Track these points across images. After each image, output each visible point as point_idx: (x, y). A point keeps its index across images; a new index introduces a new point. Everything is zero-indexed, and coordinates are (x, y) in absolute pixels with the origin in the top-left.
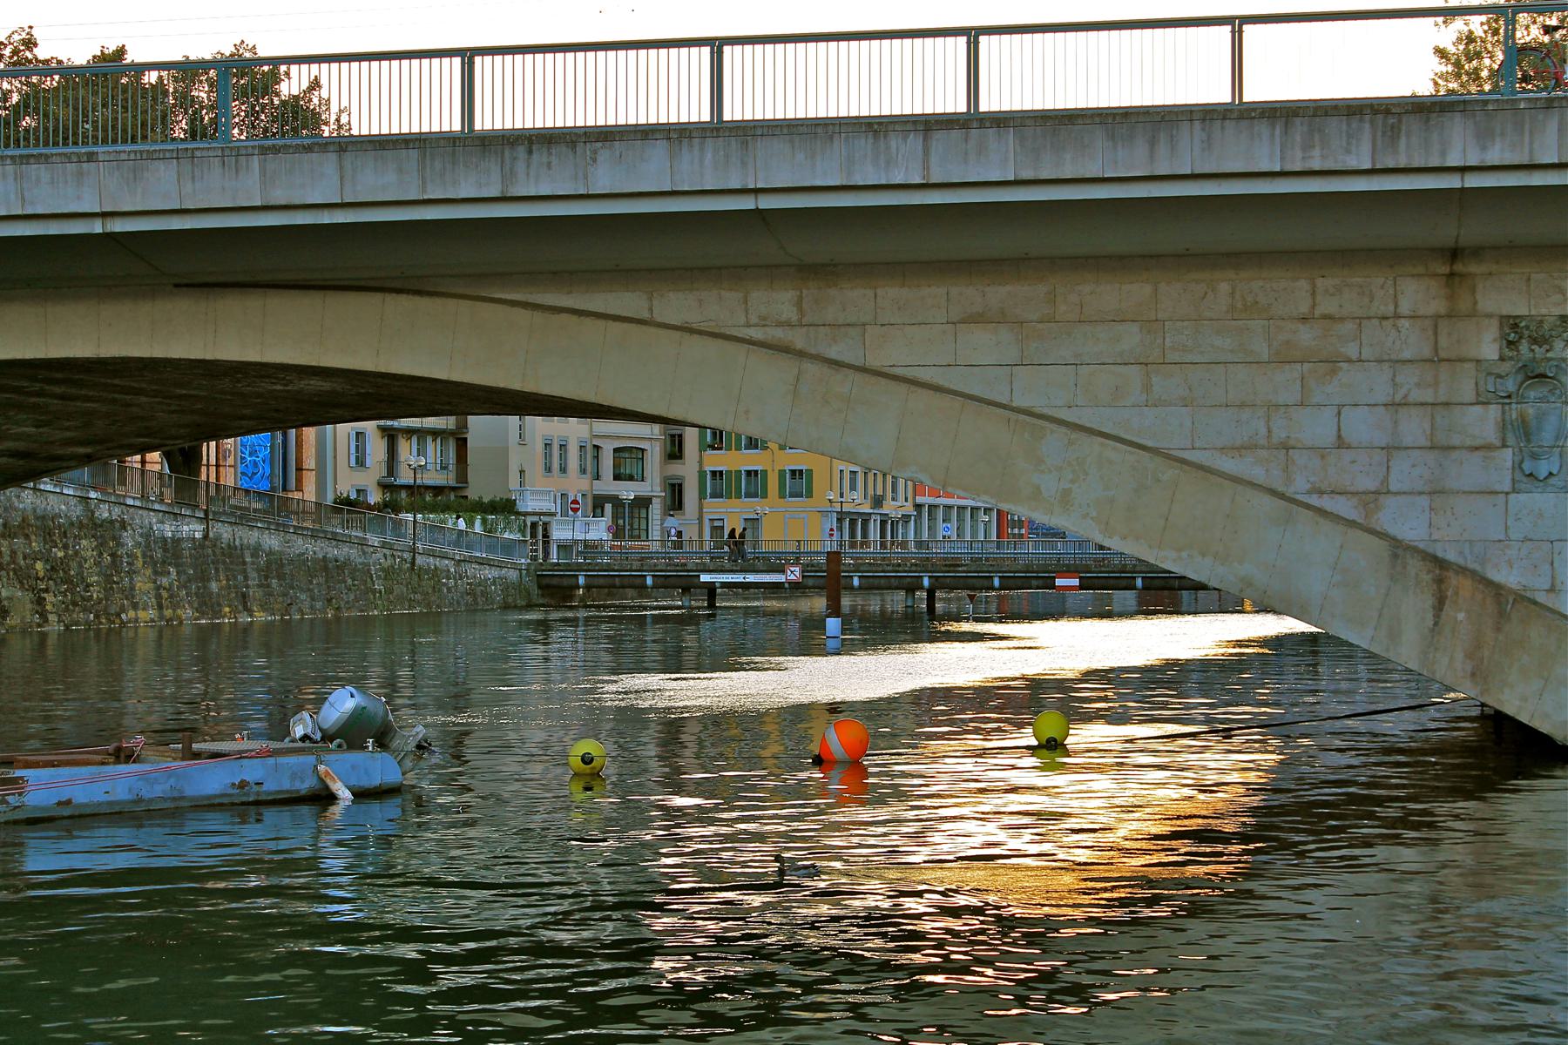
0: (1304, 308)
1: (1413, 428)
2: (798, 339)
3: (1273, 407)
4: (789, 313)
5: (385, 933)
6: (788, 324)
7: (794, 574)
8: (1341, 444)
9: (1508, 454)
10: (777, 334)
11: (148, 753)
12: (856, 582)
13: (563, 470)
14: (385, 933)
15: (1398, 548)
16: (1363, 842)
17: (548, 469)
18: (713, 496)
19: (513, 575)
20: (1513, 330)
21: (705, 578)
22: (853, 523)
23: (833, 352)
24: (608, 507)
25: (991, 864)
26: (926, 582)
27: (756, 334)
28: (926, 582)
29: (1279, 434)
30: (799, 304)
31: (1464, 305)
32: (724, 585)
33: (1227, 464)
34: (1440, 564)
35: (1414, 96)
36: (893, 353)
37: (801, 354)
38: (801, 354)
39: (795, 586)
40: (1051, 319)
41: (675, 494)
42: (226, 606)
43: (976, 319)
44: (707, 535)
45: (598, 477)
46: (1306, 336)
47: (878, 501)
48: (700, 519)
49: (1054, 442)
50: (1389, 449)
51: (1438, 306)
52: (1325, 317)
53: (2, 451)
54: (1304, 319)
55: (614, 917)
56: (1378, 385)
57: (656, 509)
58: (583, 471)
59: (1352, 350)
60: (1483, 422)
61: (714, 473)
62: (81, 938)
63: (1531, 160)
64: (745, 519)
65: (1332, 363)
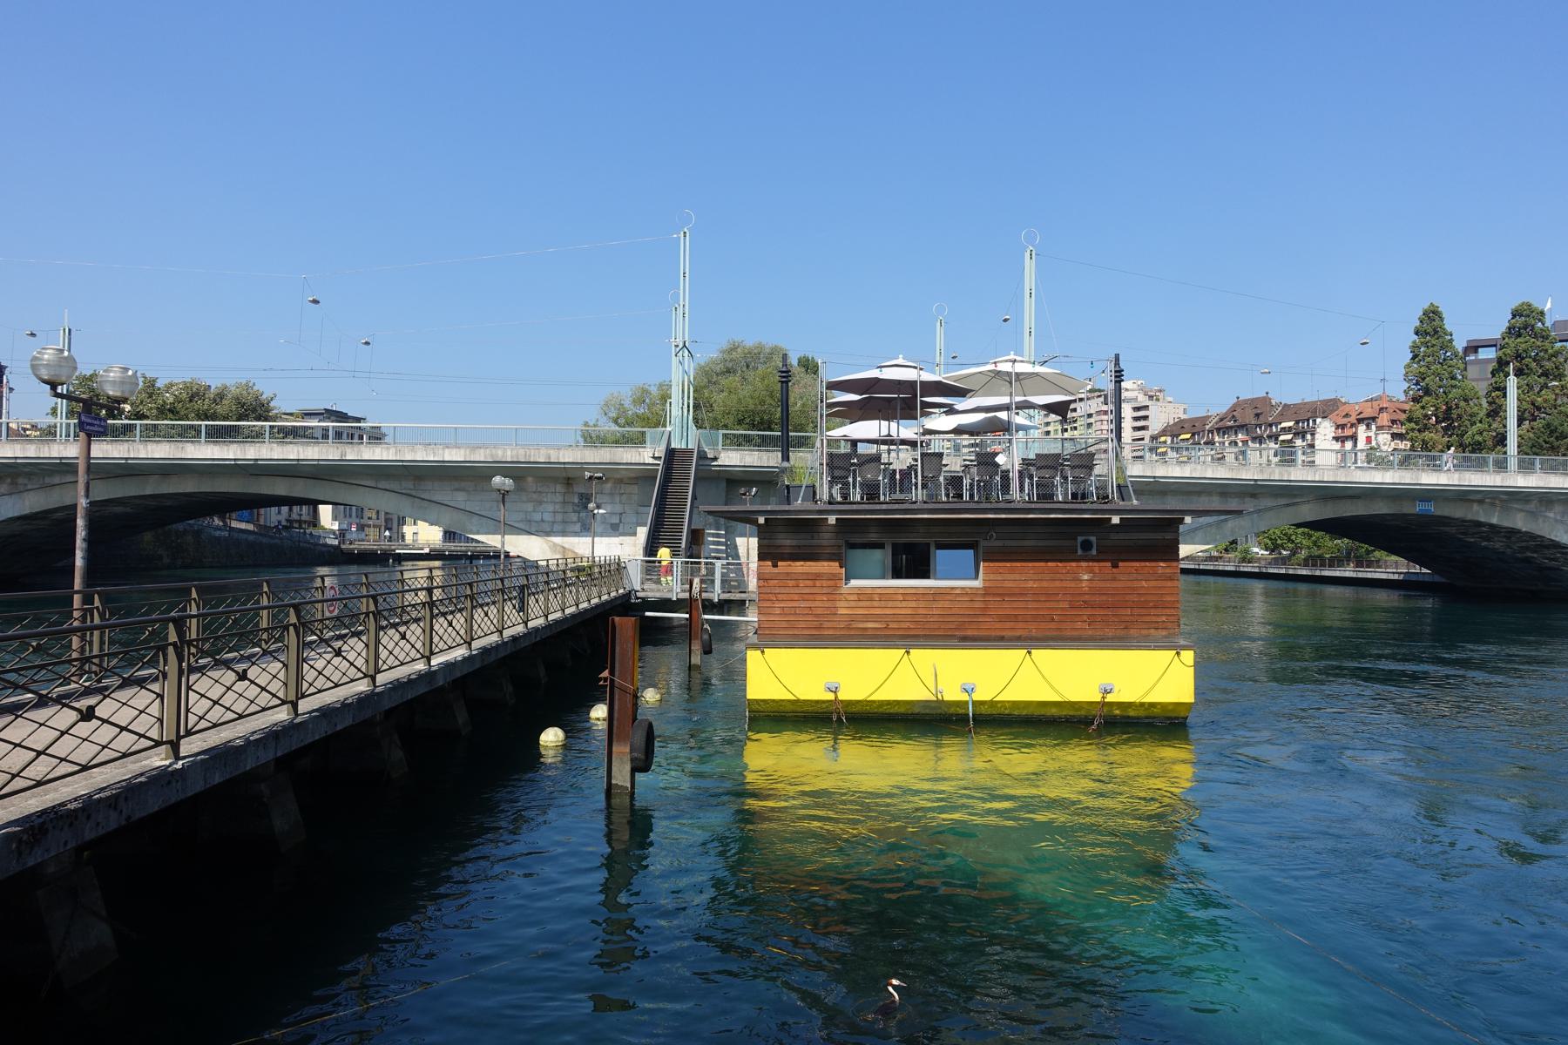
0: (534, 490)
1: (559, 517)
2: (414, 493)
3: (526, 512)
4: (412, 487)
5: (971, 720)
6: (411, 489)
8: (542, 521)
10: (408, 492)
13: (350, 516)
14: (971, 720)
16: (1295, 496)
17: (345, 516)
23: (422, 496)
27: (404, 491)
29: (528, 517)
30: (414, 484)
31: (571, 490)
33: (517, 525)
36: (437, 498)
37: (415, 497)
38: (415, 497)
40: (476, 490)
42: (1271, 430)
43: (457, 490)
45: (362, 518)
46: (535, 496)
49: (475, 519)
50: (554, 522)
51: (563, 491)
52: (540, 492)
54: (535, 492)
55: (868, 882)
56: (550, 508)
58: (357, 517)
59: (545, 500)
62: (565, 850)
63: (741, 461)
64: (814, 486)
65: (541, 503)
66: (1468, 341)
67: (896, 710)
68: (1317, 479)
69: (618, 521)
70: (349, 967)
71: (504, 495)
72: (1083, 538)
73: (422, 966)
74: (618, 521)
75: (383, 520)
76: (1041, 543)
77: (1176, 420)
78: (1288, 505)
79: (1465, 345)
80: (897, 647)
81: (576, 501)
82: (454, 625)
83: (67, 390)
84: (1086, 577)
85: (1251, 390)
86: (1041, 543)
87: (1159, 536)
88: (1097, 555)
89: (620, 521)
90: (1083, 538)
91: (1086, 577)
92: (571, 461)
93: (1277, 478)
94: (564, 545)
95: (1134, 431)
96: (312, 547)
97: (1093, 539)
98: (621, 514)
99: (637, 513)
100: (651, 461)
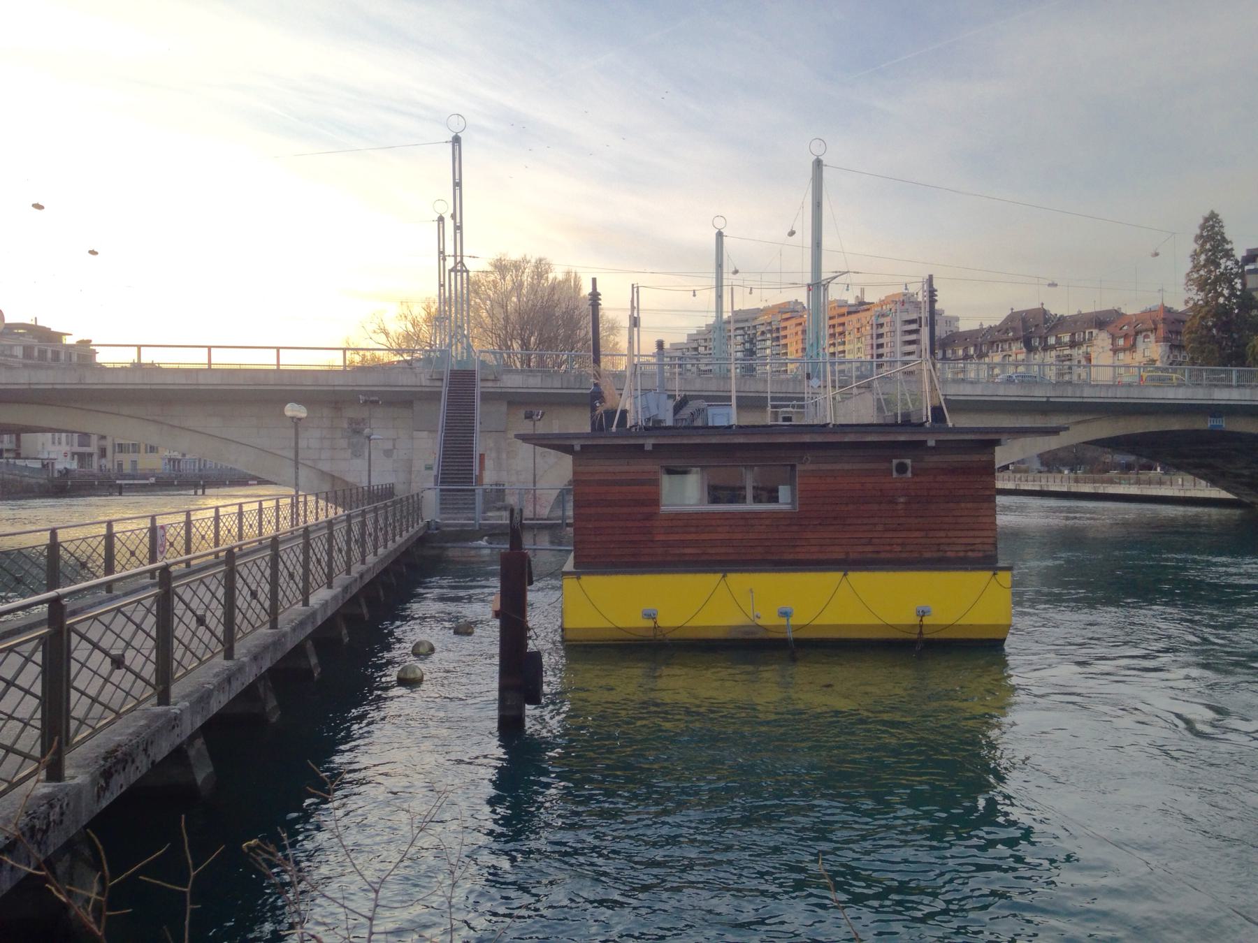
7: (153, 480)
9: (350, 451)
11: (1083, 936)
12: (176, 483)
13: (60, 443)
15: (323, 473)
17: (53, 443)
18: (119, 452)
19: (42, 481)
20: (352, 421)
21: (118, 482)
22: (174, 462)
24: (76, 456)
25: (1178, 748)
26: (202, 483)
28: (202, 483)
32: (126, 484)
33: (279, 452)
34: (333, 477)
35: (153, 364)
39: (152, 485)
41: (103, 453)
44: (116, 467)
45: (72, 445)
47: (184, 455)
48: (113, 461)
53: (1250, 603)
57: (95, 458)
60: (343, 443)
61: (119, 444)
66: (1248, 250)
67: (712, 635)
68: (1110, 396)
69: (391, 447)
70: (809, 941)
71: (296, 424)
72: (898, 461)
73: (502, 922)
74: (391, 447)
75: (96, 447)
76: (866, 466)
77: (949, 333)
78: (1079, 422)
79: (1245, 254)
80: (715, 572)
81: (346, 426)
82: (129, 553)
83: (1016, 535)
84: (902, 500)
85: (1026, 301)
86: (866, 466)
87: (976, 457)
88: (912, 478)
89: (394, 448)
90: (898, 461)
91: (902, 500)
92: (341, 383)
93: (1069, 395)
94: (334, 474)
95: (905, 345)
96: (19, 479)
97: (908, 462)
98: (394, 440)
99: (413, 438)
100: (428, 383)
